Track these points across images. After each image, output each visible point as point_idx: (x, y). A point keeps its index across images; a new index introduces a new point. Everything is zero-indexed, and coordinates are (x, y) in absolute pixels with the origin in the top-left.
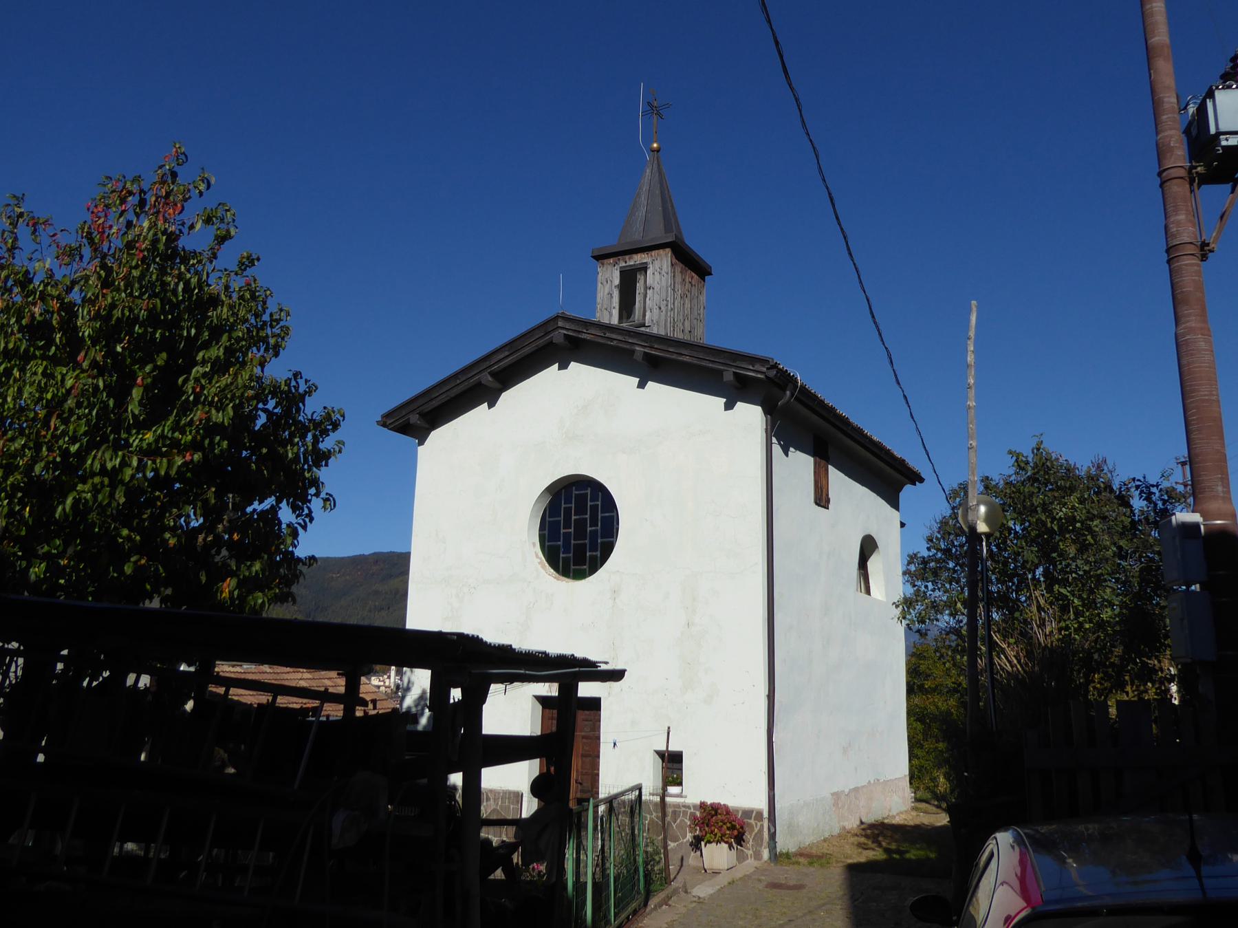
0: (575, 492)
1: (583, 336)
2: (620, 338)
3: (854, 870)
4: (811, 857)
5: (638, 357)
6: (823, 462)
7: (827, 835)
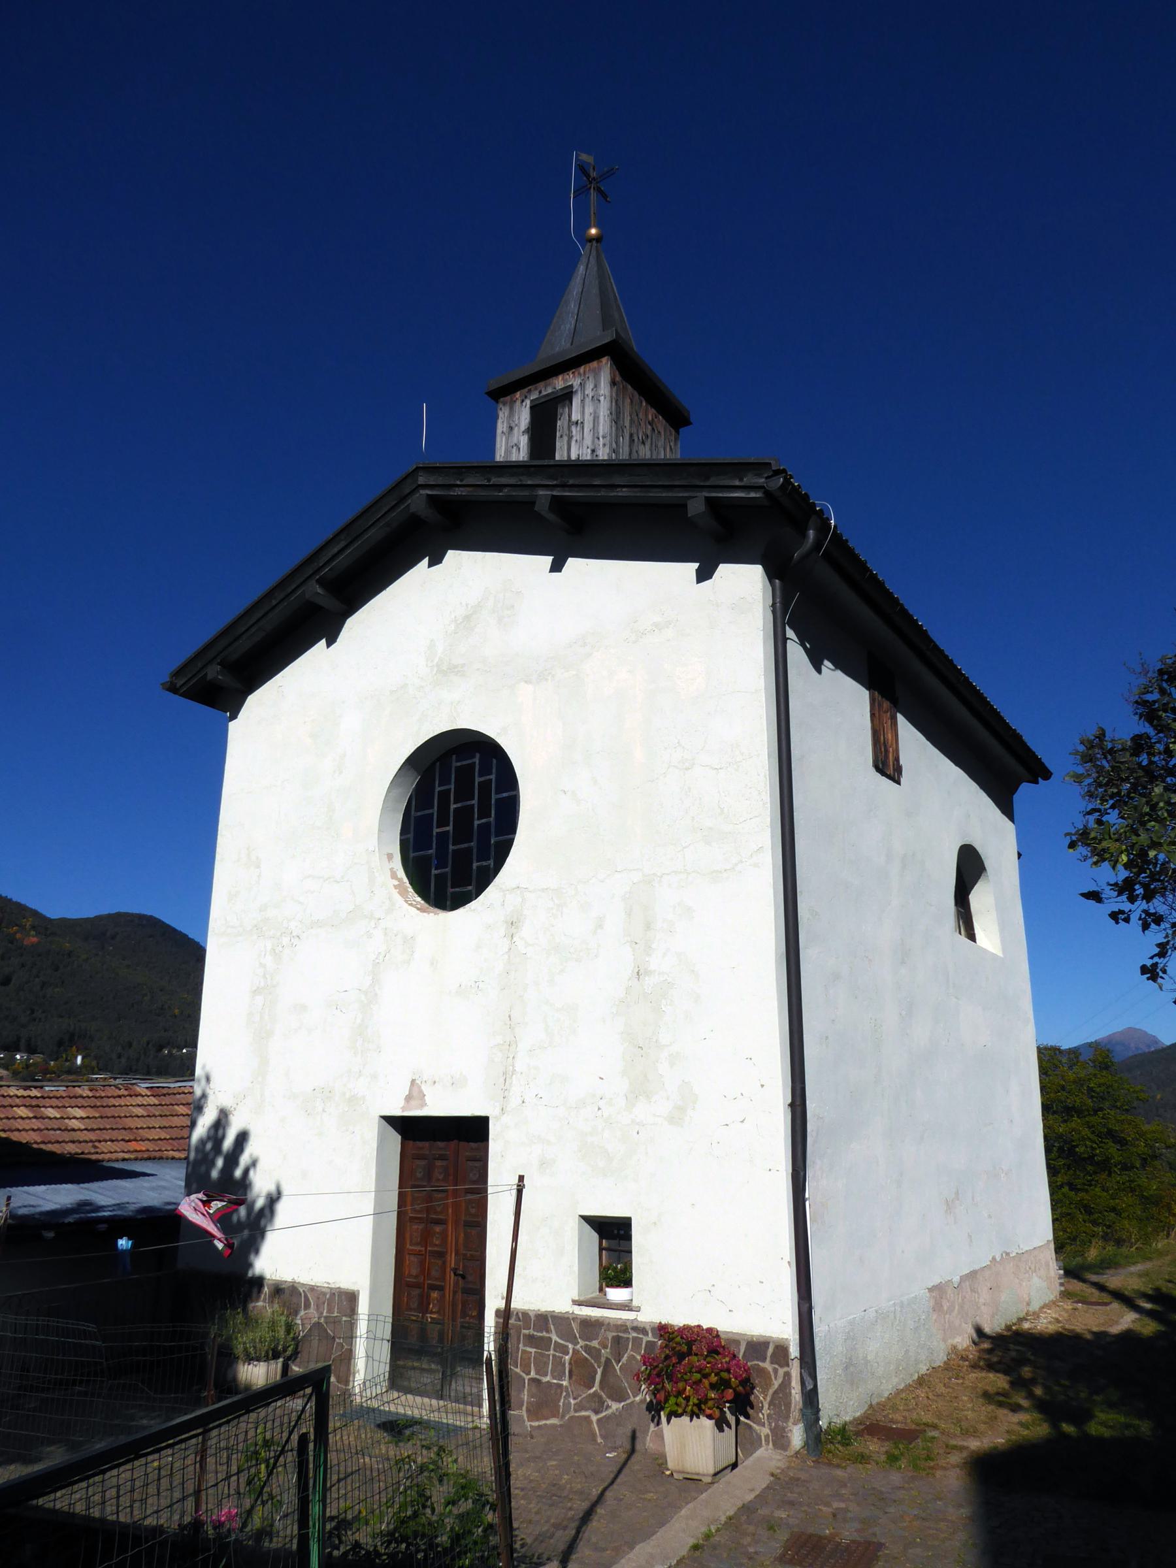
0: (455, 764)
1: (458, 492)
2: (512, 481)
3: (990, 1471)
4: (889, 1433)
5: (542, 506)
6: (886, 704)
7: (924, 1369)
